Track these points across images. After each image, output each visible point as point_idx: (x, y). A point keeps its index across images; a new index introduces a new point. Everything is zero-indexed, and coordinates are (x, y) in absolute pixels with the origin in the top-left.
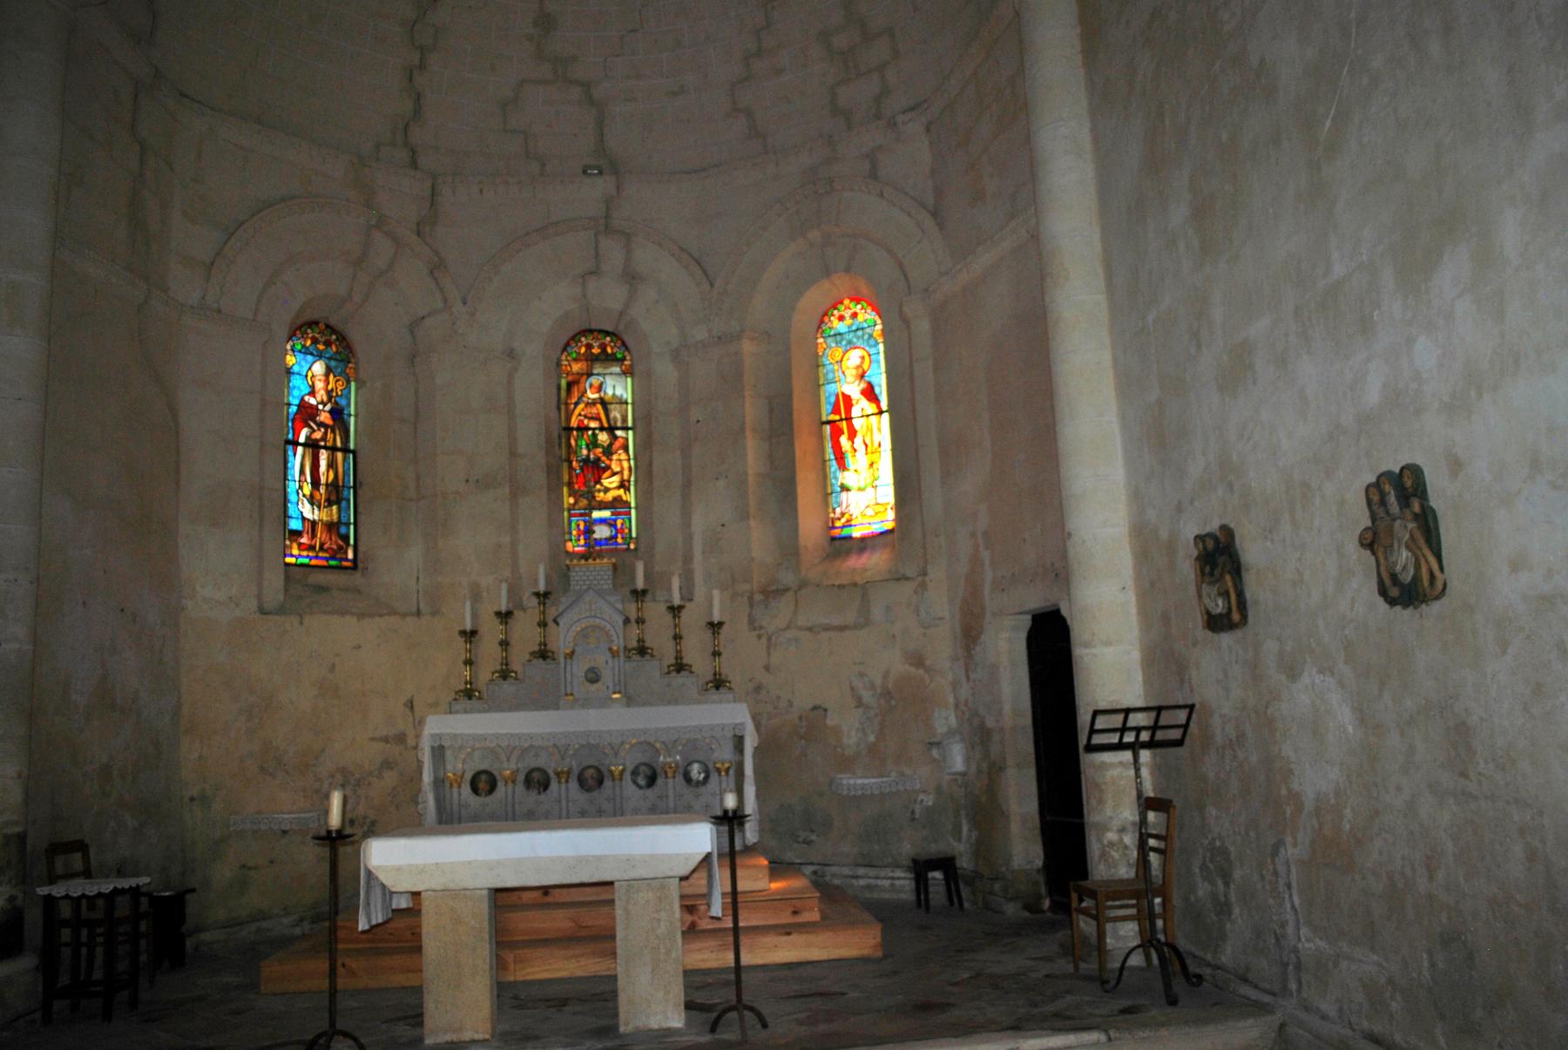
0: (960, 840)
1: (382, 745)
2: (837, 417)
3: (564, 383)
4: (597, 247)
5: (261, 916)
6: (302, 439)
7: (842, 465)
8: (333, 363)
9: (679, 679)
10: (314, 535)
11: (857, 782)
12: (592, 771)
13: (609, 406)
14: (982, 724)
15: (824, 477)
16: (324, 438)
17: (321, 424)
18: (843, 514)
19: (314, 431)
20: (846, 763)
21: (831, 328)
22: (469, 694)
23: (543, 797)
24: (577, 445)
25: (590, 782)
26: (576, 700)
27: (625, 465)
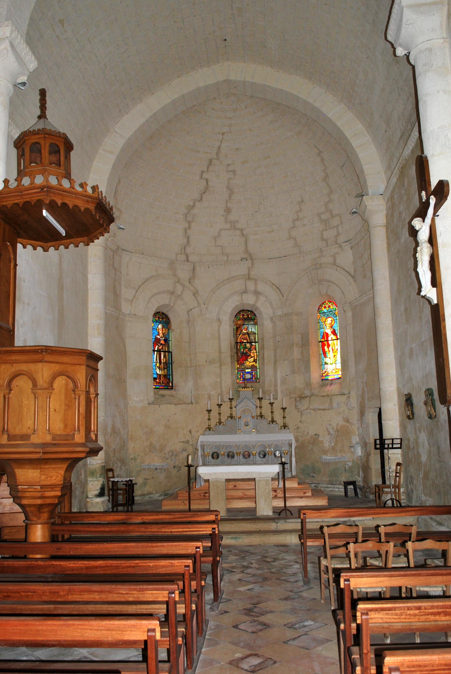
0: (359, 477)
1: (182, 444)
2: (324, 340)
4: (246, 285)
5: (150, 493)
6: (156, 349)
7: (325, 356)
8: (164, 325)
9: (272, 425)
10: (160, 379)
11: (328, 458)
12: (247, 452)
14: (365, 441)
15: (320, 360)
16: (162, 348)
17: (162, 344)
18: (325, 372)
19: (159, 346)
20: (325, 452)
21: (322, 310)
22: (209, 429)
23: (232, 460)
25: (247, 456)
26: (242, 431)
27: (255, 354)
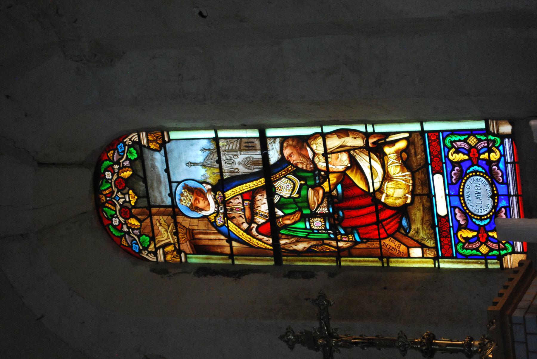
3: (196, 259)
13: (226, 175)
24: (306, 239)
